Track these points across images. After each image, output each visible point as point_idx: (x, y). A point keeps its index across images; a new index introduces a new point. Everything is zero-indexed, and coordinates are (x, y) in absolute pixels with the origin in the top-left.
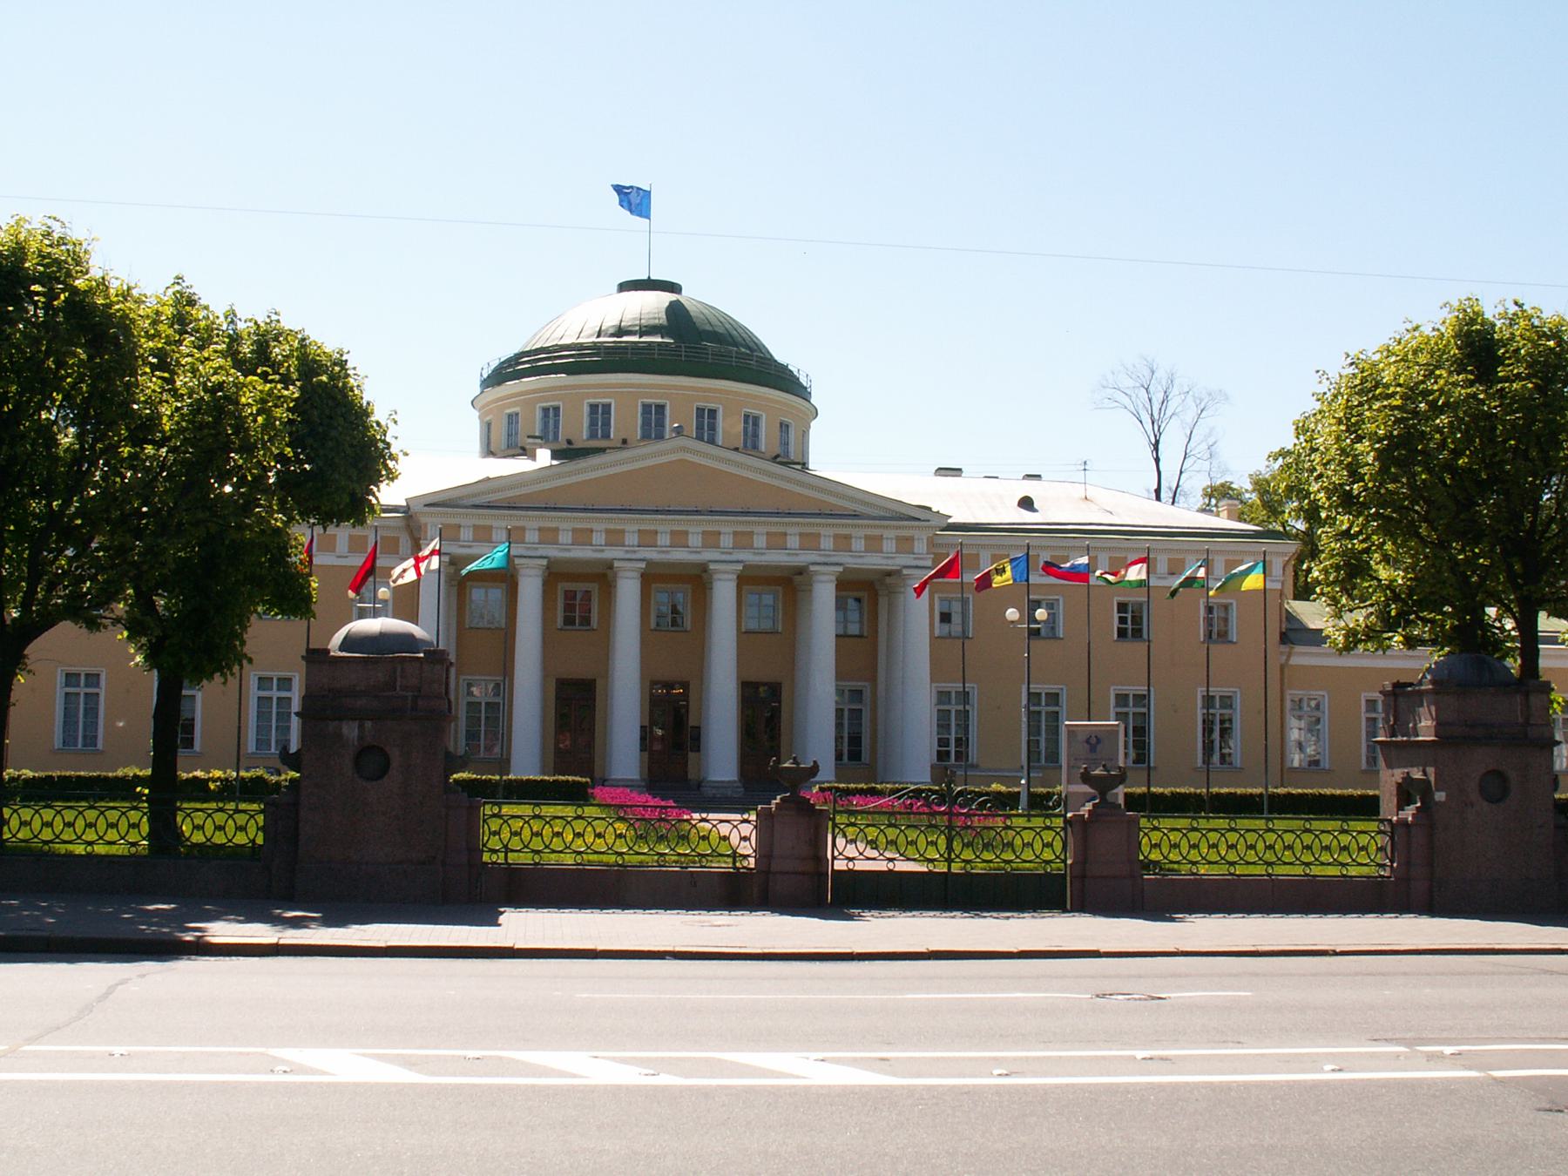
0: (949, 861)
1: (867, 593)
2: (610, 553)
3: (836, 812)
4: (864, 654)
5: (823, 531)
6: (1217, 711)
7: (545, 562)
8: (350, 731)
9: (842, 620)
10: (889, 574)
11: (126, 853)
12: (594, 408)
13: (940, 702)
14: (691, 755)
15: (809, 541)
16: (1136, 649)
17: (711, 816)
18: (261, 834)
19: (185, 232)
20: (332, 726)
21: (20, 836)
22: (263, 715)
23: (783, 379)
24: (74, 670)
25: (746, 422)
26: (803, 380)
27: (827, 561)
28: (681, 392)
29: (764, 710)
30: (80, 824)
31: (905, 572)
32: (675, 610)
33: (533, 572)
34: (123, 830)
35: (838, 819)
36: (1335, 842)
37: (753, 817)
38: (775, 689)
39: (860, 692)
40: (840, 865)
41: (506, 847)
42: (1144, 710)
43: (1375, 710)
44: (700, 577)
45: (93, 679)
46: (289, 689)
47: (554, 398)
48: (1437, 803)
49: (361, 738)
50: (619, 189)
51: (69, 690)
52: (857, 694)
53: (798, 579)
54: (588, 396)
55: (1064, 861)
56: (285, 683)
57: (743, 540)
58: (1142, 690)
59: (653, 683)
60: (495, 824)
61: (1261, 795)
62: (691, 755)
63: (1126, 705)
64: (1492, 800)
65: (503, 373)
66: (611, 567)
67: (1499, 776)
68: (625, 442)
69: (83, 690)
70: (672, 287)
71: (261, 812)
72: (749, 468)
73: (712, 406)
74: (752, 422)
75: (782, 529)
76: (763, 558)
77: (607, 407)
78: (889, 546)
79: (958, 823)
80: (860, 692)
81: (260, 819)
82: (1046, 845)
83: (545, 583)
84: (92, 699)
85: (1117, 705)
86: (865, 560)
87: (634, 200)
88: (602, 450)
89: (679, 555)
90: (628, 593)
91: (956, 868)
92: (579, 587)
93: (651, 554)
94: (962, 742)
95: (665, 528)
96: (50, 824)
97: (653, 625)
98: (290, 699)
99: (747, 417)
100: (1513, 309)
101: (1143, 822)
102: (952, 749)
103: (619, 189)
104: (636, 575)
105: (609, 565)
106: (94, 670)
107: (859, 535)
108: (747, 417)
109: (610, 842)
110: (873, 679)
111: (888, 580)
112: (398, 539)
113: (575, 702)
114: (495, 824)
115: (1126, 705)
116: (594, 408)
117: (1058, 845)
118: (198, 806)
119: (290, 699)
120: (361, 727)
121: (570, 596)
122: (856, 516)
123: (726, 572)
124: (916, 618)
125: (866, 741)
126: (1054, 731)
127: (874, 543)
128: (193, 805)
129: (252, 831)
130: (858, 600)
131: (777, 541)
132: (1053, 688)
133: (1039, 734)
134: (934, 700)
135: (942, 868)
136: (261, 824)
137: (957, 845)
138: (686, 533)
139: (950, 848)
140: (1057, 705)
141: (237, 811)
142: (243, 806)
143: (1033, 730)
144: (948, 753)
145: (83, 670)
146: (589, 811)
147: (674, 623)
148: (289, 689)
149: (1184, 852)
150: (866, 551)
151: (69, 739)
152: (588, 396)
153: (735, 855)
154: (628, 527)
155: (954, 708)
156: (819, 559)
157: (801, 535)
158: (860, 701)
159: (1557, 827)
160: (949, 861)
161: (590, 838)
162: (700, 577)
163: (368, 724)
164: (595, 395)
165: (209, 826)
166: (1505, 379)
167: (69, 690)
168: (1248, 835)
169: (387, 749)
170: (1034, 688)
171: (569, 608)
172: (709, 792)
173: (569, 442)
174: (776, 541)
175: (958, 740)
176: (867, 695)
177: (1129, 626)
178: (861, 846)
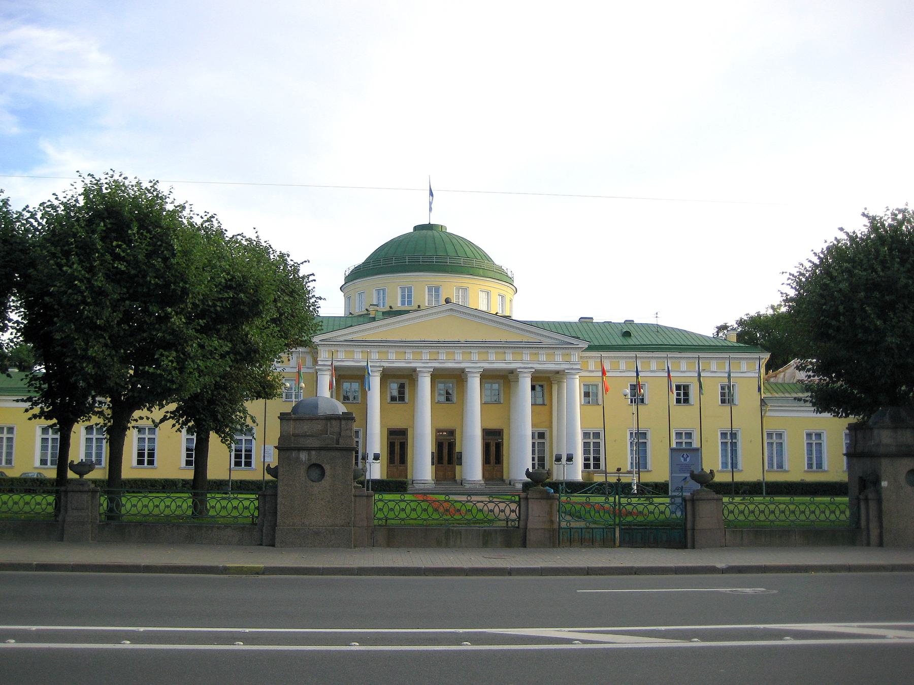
8: (303, 456)
9: (534, 397)
10: (557, 372)
14: (458, 467)
16: (727, 408)
17: (240, 496)
20: (294, 454)
21: (176, 513)
26: (510, 274)
28: (420, 285)
32: (448, 393)
38: (403, 433)
43: (726, 438)
45: (819, 436)
49: (309, 460)
52: (541, 435)
59: (438, 431)
60: (380, 505)
62: (458, 467)
65: (357, 274)
68: (419, 306)
71: (257, 499)
81: (256, 503)
82: (732, 512)
88: (407, 312)
94: (597, 459)
105: (414, 370)
111: (558, 376)
128: (154, 495)
129: (128, 506)
130: (542, 386)
136: (257, 505)
146: (408, 497)
147: (448, 399)
151: (810, 465)
153: (507, 520)
155: (592, 440)
161: (151, 504)
163: (313, 452)
168: (412, 504)
173: (391, 307)
175: (97, 454)
176: (547, 435)
177: (682, 397)
178: (646, 511)
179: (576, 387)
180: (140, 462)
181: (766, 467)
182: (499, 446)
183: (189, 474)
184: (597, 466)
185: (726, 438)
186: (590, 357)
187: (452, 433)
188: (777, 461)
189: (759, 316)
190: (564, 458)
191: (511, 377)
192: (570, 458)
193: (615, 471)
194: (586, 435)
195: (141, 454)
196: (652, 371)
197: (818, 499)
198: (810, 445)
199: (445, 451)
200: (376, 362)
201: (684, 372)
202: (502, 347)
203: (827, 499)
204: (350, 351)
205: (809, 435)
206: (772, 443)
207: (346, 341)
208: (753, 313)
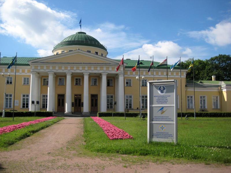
2: (100, 72)
6: (203, 99)
7: (71, 73)
13: (107, 98)
14: (82, 107)
29: (94, 100)
31: (48, 72)
33: (51, 74)
44: (99, 76)
45: (131, 97)
51: (43, 98)
53: (100, 76)
61: (13, 113)
62: (82, 107)
70: (85, 33)
72: (91, 55)
76: (57, 71)
90: (86, 78)
94: (130, 105)
97: (43, 84)
98: (11, 98)
110: (114, 94)
113: (61, 100)
115: (144, 98)
143: (7, 101)
145: (9, 94)
150: (65, 69)
155: (203, 99)
167: (43, 98)
174: (42, 68)
175: (10, 103)
176: (113, 97)
179: (121, 80)
180: (24, 107)
181: (187, 108)
182: (96, 100)
183: (15, 110)
184: (130, 107)
185: (202, 98)
186: (128, 70)
187: (80, 95)
188: (26, 105)
190: (35, 103)
191: (100, 76)
192: (33, 102)
193: (136, 109)
194: (108, 97)
195: (24, 104)
196: (174, 76)
198: (201, 100)
199: (78, 102)
200: (86, 72)
201: (175, 76)
202: (96, 64)
204: (89, 67)
205: (201, 97)
206: (189, 100)
207: (41, 63)
208: (227, 54)
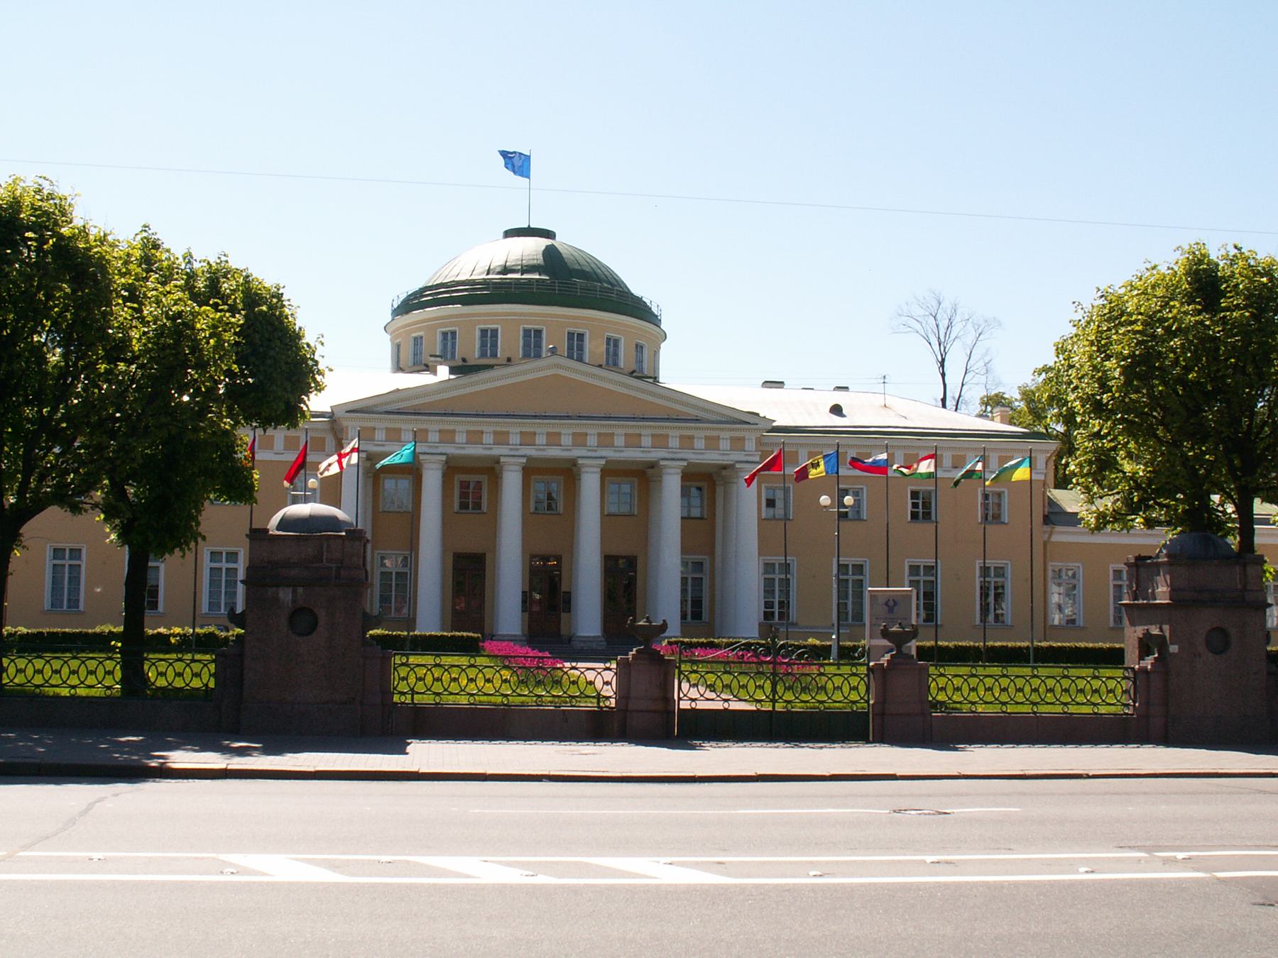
0: (774, 701)
1: (706, 483)
2: (497, 451)
3: (681, 661)
4: (704, 532)
5: (671, 433)
6: (992, 579)
7: (444, 458)
8: (286, 595)
9: (687, 505)
10: (725, 467)
11: (103, 695)
12: (484, 332)
13: (766, 572)
14: (563, 615)
15: (660, 441)
16: (926, 529)
17: (580, 665)
18: (212, 679)
19: (151, 189)
20: (270, 591)
21: (16, 681)
22: (214, 583)
23: (638, 309)
24: (60, 545)
25: (608, 344)
26: (654, 310)
27: (674, 457)
28: (555, 319)
29: (623, 578)
30: (65, 671)
31: (738, 466)
32: (550, 497)
33: (434, 466)
34: (100, 676)
35: (683, 667)
36: (1088, 686)
37: (614, 666)
38: (632, 562)
39: (701, 564)
40: (685, 705)
41: (412, 690)
42: (932, 578)
43: (1121, 579)
44: (570, 470)
45: (76, 553)
46: (236, 562)
47: (452, 324)
48: (1171, 654)
49: (294, 601)
50: (504, 154)
51: (56, 562)
52: (698, 566)
53: (650, 471)
54: (479, 322)
55: (867, 702)
56: (232, 556)
57: (606, 440)
58: (931, 562)
59: (533, 557)
60: (403, 672)
61: (1028, 648)
62: (563, 615)
63: (918, 574)
64: (1216, 652)
65: (410, 304)
66: (498, 462)
67: (1221, 632)
68: (509, 360)
69: (67, 562)
70: (548, 234)
71: (213, 661)
72: (610, 381)
73: (580, 331)
74: (613, 344)
75: (637, 431)
76: (622, 455)
77: (495, 332)
78: (725, 445)
79: (781, 670)
80: (701, 564)
81: (212, 667)
82: (852, 689)
83: (444, 475)
84: (75, 569)
85: (911, 574)
86: (705, 457)
87: (517, 163)
88: (491, 367)
89: (554, 452)
90: (512, 483)
91: (779, 707)
92: (472, 478)
93: (531, 451)
94: (784, 605)
95: (542, 430)
96: (40, 672)
97: (532, 509)
98: (236, 569)
99: (609, 339)
100: (1233, 252)
101: (932, 670)
102: (776, 610)
103: (504, 154)
104: (519, 468)
105: (496, 460)
106: (76, 546)
107: (700, 436)
108: (609, 339)
109: (497, 686)
110: (712, 553)
111: (724, 473)
112: (324, 439)
113: (469, 572)
114: (403, 672)
115: (918, 574)
116: (484, 332)
117: (862, 688)
118: (162, 656)
119: (236, 569)
120: (294, 592)
121: (464, 485)
122: (697, 420)
123: (591, 466)
124: (747, 503)
125: (706, 604)
126: (859, 595)
127: (712, 443)
128: (157, 656)
130: (700, 489)
131: (633, 441)
132: (858, 561)
133: (847, 598)
134: (762, 571)
135: (768, 707)
136: (213, 671)
137: (780, 688)
138: (559, 434)
139: (774, 691)
140: (862, 574)
141: (193, 661)
142: (198, 657)
143: (842, 595)
144: (773, 613)
145: (68, 546)
146: (480, 661)
147: (550, 507)
148: (236, 562)
149: (965, 694)
150: (706, 449)
151: (56, 602)
152: (479, 322)
153: (599, 697)
154: (512, 430)
155: (777, 577)
156: (667, 456)
157: (653, 436)
158: (701, 571)
159: (1269, 674)
160: (774, 701)
162: (570, 470)
163: (300, 590)
164: (485, 322)
165: (170, 673)
166: (1227, 309)
167: (56, 562)
168: (1017, 681)
169: (315, 610)
170: (843, 560)
171: (464, 495)
172: (578, 645)
173: (464, 360)
174: (633, 441)
175: (781, 603)
176: (707, 566)
177: (920, 510)
178: (702, 689)
189: (298, 336)
197: (447, 660)
203: (429, 660)
